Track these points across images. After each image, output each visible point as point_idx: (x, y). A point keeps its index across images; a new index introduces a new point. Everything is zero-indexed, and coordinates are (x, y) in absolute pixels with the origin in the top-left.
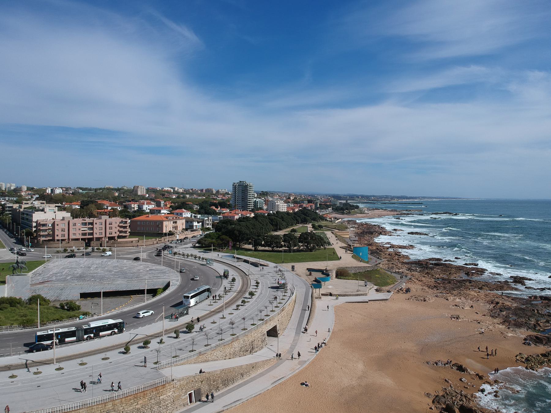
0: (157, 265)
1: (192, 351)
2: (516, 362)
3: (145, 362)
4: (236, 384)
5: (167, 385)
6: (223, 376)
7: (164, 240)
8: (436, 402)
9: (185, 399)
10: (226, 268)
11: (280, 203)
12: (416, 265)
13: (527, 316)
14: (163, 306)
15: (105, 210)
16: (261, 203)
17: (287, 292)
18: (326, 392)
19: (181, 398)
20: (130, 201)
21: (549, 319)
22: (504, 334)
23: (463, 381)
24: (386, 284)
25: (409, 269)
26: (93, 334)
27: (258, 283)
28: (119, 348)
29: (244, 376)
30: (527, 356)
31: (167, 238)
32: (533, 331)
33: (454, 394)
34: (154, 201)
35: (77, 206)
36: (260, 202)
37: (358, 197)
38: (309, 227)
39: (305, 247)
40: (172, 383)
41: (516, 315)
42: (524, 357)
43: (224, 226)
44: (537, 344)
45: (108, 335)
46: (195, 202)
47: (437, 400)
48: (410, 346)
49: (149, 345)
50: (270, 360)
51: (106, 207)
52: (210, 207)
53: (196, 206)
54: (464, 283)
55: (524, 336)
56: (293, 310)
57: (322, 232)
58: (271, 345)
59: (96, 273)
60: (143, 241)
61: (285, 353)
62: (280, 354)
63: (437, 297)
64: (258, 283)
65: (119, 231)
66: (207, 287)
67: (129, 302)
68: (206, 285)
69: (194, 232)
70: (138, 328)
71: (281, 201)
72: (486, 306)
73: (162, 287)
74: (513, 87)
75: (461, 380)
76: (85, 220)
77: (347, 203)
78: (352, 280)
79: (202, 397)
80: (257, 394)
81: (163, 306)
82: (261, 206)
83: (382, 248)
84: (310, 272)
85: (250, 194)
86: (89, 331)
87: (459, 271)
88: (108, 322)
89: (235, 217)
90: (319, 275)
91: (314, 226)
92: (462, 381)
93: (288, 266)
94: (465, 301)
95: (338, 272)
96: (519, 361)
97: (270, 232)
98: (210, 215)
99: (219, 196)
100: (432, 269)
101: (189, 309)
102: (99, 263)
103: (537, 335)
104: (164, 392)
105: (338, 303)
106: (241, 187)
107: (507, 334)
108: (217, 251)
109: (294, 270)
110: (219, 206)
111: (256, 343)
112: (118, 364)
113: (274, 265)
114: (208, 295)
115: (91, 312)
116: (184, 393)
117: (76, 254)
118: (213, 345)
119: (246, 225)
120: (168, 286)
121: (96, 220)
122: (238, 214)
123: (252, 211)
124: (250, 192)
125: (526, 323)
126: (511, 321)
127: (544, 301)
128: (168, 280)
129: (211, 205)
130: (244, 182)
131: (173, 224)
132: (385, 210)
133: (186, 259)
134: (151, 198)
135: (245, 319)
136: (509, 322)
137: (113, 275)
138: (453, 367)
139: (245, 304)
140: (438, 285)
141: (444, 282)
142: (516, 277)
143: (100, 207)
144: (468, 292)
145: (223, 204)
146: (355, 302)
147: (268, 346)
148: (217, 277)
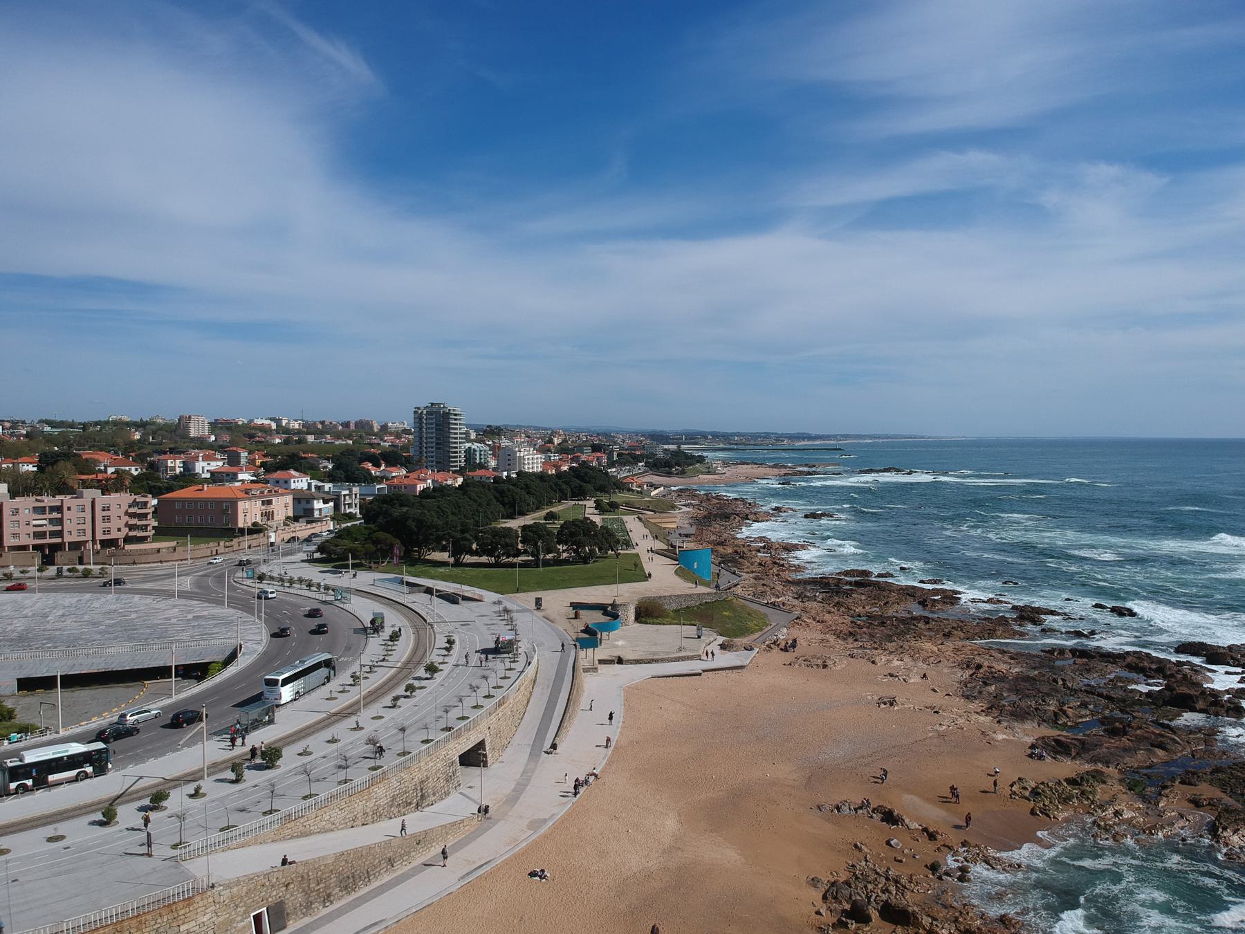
0: (214, 605)
1: (271, 812)
2: (1011, 798)
3: (149, 846)
4: (375, 884)
5: (198, 899)
6: (341, 868)
7: (239, 546)
8: (830, 898)
9: (244, 928)
10: (379, 608)
11: (526, 453)
12: (815, 586)
13: (1040, 694)
14: (203, 707)
15: (99, 475)
16: (482, 453)
17: (518, 659)
18: (587, 889)
19: (235, 927)
20: (165, 453)
21: (1087, 700)
22: (988, 735)
23: (894, 845)
24: (744, 631)
25: (799, 596)
26: (31, 780)
27: (450, 642)
28: (93, 811)
29: (395, 865)
30: (1033, 784)
31: (246, 540)
32: (1052, 727)
33: (872, 876)
34: (224, 452)
35: (31, 466)
36: (481, 451)
37: (706, 438)
38: (589, 507)
39: (573, 554)
40: (209, 893)
41: (1017, 692)
42: (1028, 787)
43: (384, 509)
44: (1058, 757)
45: (70, 781)
46: (323, 452)
47: (832, 893)
48: (785, 772)
49: (164, 803)
50: (462, 821)
51: (103, 468)
52: (360, 463)
53: (325, 463)
54: (914, 625)
55: (1030, 740)
56: (528, 702)
57: (616, 518)
58: (470, 787)
59: (60, 629)
60: (185, 548)
61: (500, 804)
62: (487, 807)
63: (852, 657)
64: (450, 642)
65: (127, 525)
66: (325, 656)
67: (137, 697)
68: (323, 653)
69: (314, 525)
70: (144, 762)
71: (528, 449)
72: (955, 673)
73: (221, 658)
74: (1051, 198)
75: (888, 843)
76: (43, 501)
77: (680, 450)
78: (670, 624)
79: (289, 921)
80: (424, 905)
81: (203, 707)
82: (482, 461)
83: (746, 551)
84: (576, 612)
85: (456, 434)
86: (22, 773)
87: (906, 599)
88: (67, 751)
89: (418, 486)
90: (596, 617)
91: (599, 506)
92: (891, 845)
93: (528, 599)
94: (911, 663)
95: (640, 608)
96: (1018, 795)
97: (496, 520)
98: (356, 484)
99: (386, 438)
100: (848, 594)
101: (276, 710)
102: (71, 604)
103: (1059, 736)
104: (188, 915)
105: (633, 680)
106: (434, 416)
107: (994, 735)
108: (365, 568)
109: (539, 609)
110: (382, 462)
111: (431, 783)
112: (83, 852)
113: (495, 597)
114: (328, 675)
115: (39, 725)
116: (242, 915)
117: (28, 584)
118: (322, 796)
119: (438, 507)
120: (232, 657)
121: (67, 500)
122: (425, 480)
123: (461, 472)
124: (456, 429)
125: (1037, 709)
126: (1004, 706)
127: (1079, 661)
128: (232, 643)
129: (362, 461)
130: (442, 406)
131: (263, 507)
132: (761, 464)
133: (287, 590)
134: (221, 443)
135: (404, 731)
136: (1001, 709)
137: (101, 633)
138: (874, 815)
139: (413, 694)
140: (857, 630)
141: (872, 624)
142: (1023, 607)
143: (86, 467)
144: (919, 644)
145: (392, 458)
146: (673, 676)
147: (462, 789)
148: (356, 631)
